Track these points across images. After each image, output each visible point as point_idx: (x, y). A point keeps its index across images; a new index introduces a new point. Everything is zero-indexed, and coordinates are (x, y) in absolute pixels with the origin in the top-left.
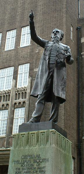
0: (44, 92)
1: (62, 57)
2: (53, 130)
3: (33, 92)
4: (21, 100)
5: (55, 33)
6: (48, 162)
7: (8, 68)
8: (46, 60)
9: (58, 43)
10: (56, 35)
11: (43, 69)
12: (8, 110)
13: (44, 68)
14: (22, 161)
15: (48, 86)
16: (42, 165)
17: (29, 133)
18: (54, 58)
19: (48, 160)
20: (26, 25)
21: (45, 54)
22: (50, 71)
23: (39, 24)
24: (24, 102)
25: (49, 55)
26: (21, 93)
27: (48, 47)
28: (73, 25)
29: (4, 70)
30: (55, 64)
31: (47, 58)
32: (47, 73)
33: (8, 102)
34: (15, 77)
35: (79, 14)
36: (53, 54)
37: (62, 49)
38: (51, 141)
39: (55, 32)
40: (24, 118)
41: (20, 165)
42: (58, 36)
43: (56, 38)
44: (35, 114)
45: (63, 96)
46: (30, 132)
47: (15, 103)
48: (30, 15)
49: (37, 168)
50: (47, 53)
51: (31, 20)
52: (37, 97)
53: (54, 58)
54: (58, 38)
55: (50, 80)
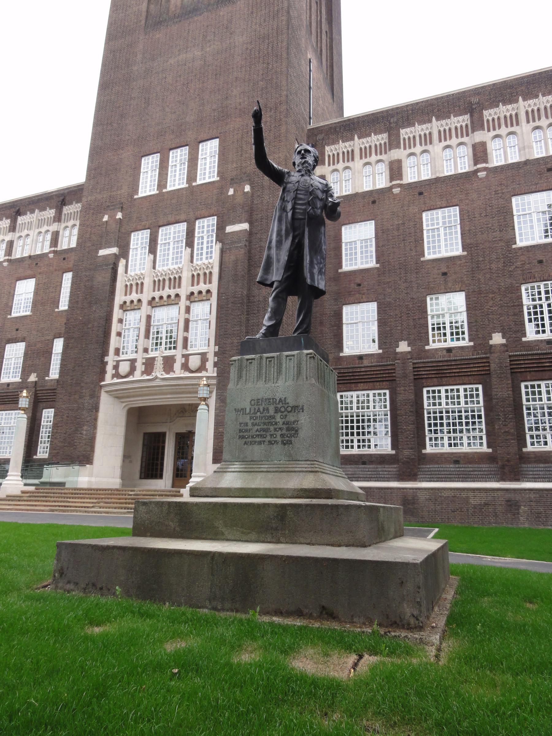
0: (285, 276)
1: (319, 206)
2: (311, 351)
3: (261, 277)
4: (203, 287)
5: (303, 155)
6: (303, 411)
7: (174, 225)
8: (286, 211)
9: (310, 176)
10: (306, 158)
11: (281, 230)
12: (177, 306)
13: (284, 228)
14: (250, 409)
15: (292, 264)
16: (291, 418)
17: (261, 358)
18: (303, 207)
19: (303, 409)
20: (209, 138)
21: (283, 199)
22: (296, 233)
23: (233, 135)
24: (208, 291)
25: (293, 202)
26: (201, 273)
27: (290, 183)
28: (299, 141)
29: (168, 227)
30: (305, 219)
31: (289, 206)
32: (290, 238)
33: (177, 291)
34: (190, 243)
35: (310, 118)
36: (301, 199)
37: (319, 189)
38: (308, 373)
39: (303, 152)
40: (208, 321)
41: (248, 417)
42: (310, 162)
43: (304, 166)
44: (270, 319)
45: (322, 285)
46: (265, 355)
47: (192, 293)
48: (255, 110)
49: (281, 423)
50: (289, 197)
51: (255, 123)
52: (271, 285)
53: (303, 207)
54: (309, 164)
55: (296, 252)
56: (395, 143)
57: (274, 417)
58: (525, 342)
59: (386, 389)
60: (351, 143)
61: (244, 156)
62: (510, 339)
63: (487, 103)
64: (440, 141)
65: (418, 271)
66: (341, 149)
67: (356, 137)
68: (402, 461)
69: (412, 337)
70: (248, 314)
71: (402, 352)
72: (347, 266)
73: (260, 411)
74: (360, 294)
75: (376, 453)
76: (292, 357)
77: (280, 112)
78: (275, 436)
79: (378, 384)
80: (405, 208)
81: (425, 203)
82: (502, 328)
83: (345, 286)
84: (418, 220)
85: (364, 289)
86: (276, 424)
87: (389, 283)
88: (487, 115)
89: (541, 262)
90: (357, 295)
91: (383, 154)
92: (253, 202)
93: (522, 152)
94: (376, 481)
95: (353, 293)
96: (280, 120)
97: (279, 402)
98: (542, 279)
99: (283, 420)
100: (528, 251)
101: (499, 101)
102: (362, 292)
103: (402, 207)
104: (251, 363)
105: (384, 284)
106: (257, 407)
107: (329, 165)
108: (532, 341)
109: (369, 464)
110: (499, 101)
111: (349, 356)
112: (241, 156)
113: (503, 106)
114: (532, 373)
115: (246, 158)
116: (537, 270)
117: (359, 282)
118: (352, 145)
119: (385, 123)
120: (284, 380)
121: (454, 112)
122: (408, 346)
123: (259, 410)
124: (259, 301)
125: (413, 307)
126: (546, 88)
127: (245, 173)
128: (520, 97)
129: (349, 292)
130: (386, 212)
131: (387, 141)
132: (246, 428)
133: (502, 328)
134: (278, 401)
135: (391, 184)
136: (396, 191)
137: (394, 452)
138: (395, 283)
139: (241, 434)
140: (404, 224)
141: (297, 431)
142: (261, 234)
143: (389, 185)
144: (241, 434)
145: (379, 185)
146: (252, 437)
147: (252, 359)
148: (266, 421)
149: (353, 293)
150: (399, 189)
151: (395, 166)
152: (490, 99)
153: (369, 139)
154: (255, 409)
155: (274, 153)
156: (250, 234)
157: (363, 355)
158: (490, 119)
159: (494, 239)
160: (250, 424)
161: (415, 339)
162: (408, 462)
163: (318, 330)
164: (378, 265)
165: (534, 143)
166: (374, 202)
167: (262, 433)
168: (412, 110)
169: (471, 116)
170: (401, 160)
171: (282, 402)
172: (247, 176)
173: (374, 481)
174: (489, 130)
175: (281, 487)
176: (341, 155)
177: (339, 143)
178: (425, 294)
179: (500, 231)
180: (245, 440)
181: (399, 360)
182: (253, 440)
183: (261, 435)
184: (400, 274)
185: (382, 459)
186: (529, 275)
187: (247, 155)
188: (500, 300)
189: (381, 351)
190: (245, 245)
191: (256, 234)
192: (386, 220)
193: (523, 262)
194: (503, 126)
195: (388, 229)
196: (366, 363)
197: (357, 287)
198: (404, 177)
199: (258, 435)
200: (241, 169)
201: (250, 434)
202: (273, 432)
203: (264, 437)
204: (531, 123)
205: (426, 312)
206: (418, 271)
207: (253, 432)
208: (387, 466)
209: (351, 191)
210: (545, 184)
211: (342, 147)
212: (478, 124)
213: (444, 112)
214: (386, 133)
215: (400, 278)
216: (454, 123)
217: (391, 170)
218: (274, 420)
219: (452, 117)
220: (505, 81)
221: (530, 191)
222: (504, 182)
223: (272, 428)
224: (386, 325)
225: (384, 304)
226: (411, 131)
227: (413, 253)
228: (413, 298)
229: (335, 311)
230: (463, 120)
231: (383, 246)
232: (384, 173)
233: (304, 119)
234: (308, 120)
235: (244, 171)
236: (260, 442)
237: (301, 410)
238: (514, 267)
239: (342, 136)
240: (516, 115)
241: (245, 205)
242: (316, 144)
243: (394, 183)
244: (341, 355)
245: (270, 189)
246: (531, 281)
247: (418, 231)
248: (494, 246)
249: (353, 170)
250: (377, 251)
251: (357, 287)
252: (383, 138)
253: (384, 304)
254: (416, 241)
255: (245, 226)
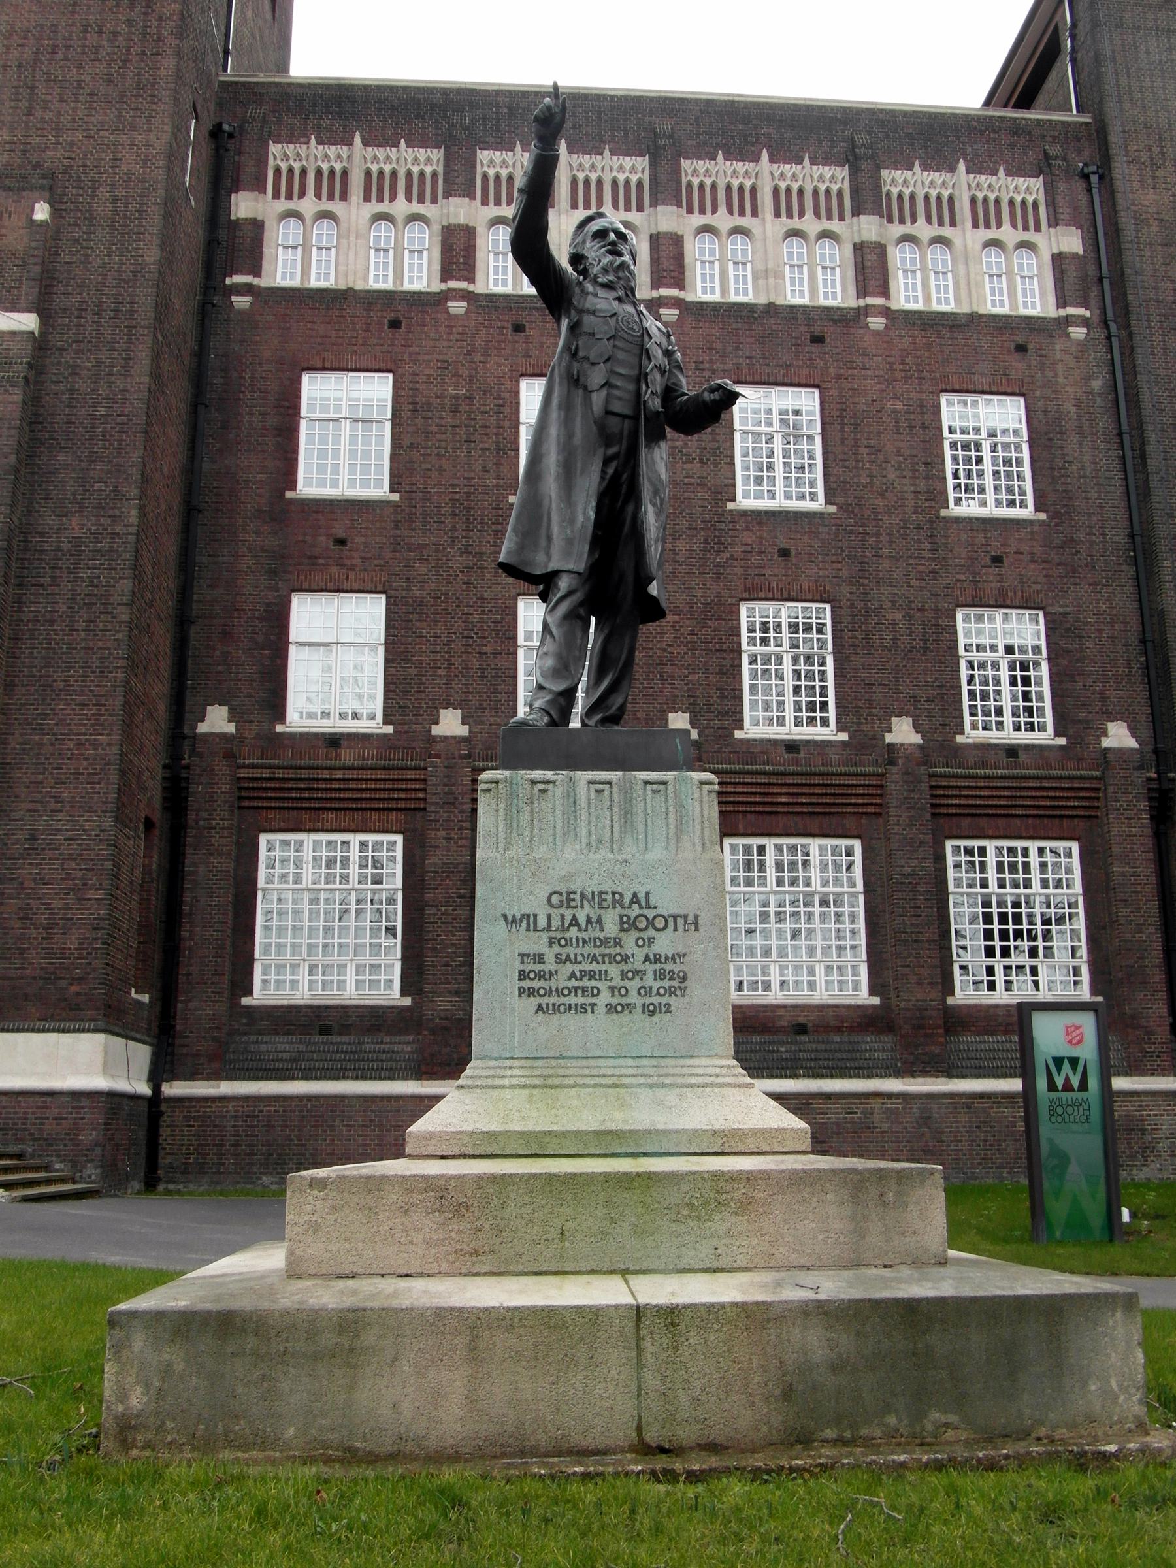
6: (697, 929)
14: (549, 917)
56: (461, 180)
57: (618, 942)
58: (741, 740)
59: (396, 832)
60: (344, 151)
61: (39, 114)
62: (707, 731)
63: (689, 143)
64: (575, 206)
65: (500, 527)
66: (312, 158)
67: (357, 139)
68: (431, 1025)
69: (474, 700)
70: (20, 585)
71: (446, 738)
72: (310, 484)
73: (577, 925)
74: (342, 565)
75: (362, 1003)
76: (661, 787)
77: (160, 19)
78: (623, 991)
79: (375, 816)
80: (478, 358)
81: (527, 356)
82: (691, 700)
83: (301, 538)
84: (507, 395)
85: (355, 554)
86: (626, 959)
87: (421, 547)
88: (689, 172)
89: (785, 553)
90: (334, 569)
91: (428, 203)
92: (57, 254)
93: (761, 282)
94: (357, 1078)
95: (321, 561)
96: (159, 39)
97: (632, 902)
98: (785, 595)
99: (646, 950)
100: (760, 523)
101: (717, 144)
102: (348, 562)
103: (469, 353)
104: (544, 791)
105: (410, 550)
106: (568, 914)
107: (276, 196)
108: (755, 740)
109: (341, 1034)
110: (717, 147)
111: (302, 734)
112: (29, 114)
113: (726, 159)
114: (749, 816)
115: (43, 120)
116: (776, 571)
117: (341, 534)
118: (345, 157)
119: (437, 121)
120: (642, 846)
121: (613, 140)
122: (463, 723)
123: (574, 922)
124: (59, 549)
125: (482, 621)
126: (820, 146)
127: (37, 165)
128: (765, 150)
129: (310, 558)
130: (427, 357)
131: (440, 170)
132: (538, 967)
133: (691, 700)
134: (627, 900)
135: (443, 286)
136: (457, 307)
137: (407, 1001)
138: (437, 551)
139: (526, 984)
140: (471, 398)
141: (684, 979)
142: (77, 352)
143: (437, 287)
144: (526, 984)
145: (411, 281)
146: (559, 993)
147: (548, 782)
148: (597, 951)
149: (321, 561)
150: (465, 304)
151: (458, 242)
152: (698, 135)
153: (393, 152)
154: (563, 917)
155: (133, 128)
156: (40, 348)
157: (342, 734)
158: (696, 182)
159: (686, 480)
160: (550, 957)
161: (481, 707)
162: (446, 1029)
163: (217, 653)
164: (396, 497)
165: (787, 267)
166: (395, 324)
167: (586, 982)
168: (510, 109)
169: (653, 164)
170: (475, 228)
171: (638, 902)
172: (44, 177)
173: (352, 1078)
174: (690, 211)
175: (681, 1127)
176: (311, 177)
177: (307, 143)
178: (513, 592)
179: (701, 461)
180: (538, 1000)
181: (438, 756)
182: (562, 1000)
183: (584, 990)
184: (454, 529)
185: (373, 1020)
186: (757, 581)
187: (48, 115)
188: (692, 633)
189: (389, 729)
190: (26, 378)
191: (62, 349)
192: (425, 379)
193: (749, 548)
194: (722, 209)
195: (429, 404)
196: (347, 756)
197: (333, 549)
198: (479, 276)
199: (576, 988)
200: (24, 152)
201: (553, 984)
202: (617, 982)
203: (593, 995)
204: (784, 218)
205: (515, 638)
206: (500, 527)
207: (561, 981)
208: (387, 1039)
209: (332, 281)
210: (805, 371)
211: (318, 155)
212: (666, 188)
213: (587, 134)
214: (438, 147)
215: (453, 539)
216: (611, 169)
217: (447, 250)
218: (618, 950)
219: (607, 153)
220: (733, 102)
221: (772, 379)
222: (719, 346)
223: (614, 971)
224: (407, 660)
225: (407, 604)
226: (504, 161)
227: (491, 481)
228: (482, 598)
229: (268, 605)
230: (633, 170)
231: (412, 446)
232: (425, 253)
233: (214, 50)
234: (221, 55)
235: (34, 158)
236: (583, 1006)
237: (693, 927)
238: (728, 555)
239: (319, 126)
240: (753, 189)
241: (32, 260)
242: (241, 127)
243: (453, 284)
244: (279, 728)
245: (112, 227)
246: (761, 595)
247: (507, 424)
248: (686, 495)
249: (344, 225)
250: (394, 457)
251: (333, 549)
252: (428, 160)
253: (407, 604)
254: (498, 450)
255: (28, 322)
